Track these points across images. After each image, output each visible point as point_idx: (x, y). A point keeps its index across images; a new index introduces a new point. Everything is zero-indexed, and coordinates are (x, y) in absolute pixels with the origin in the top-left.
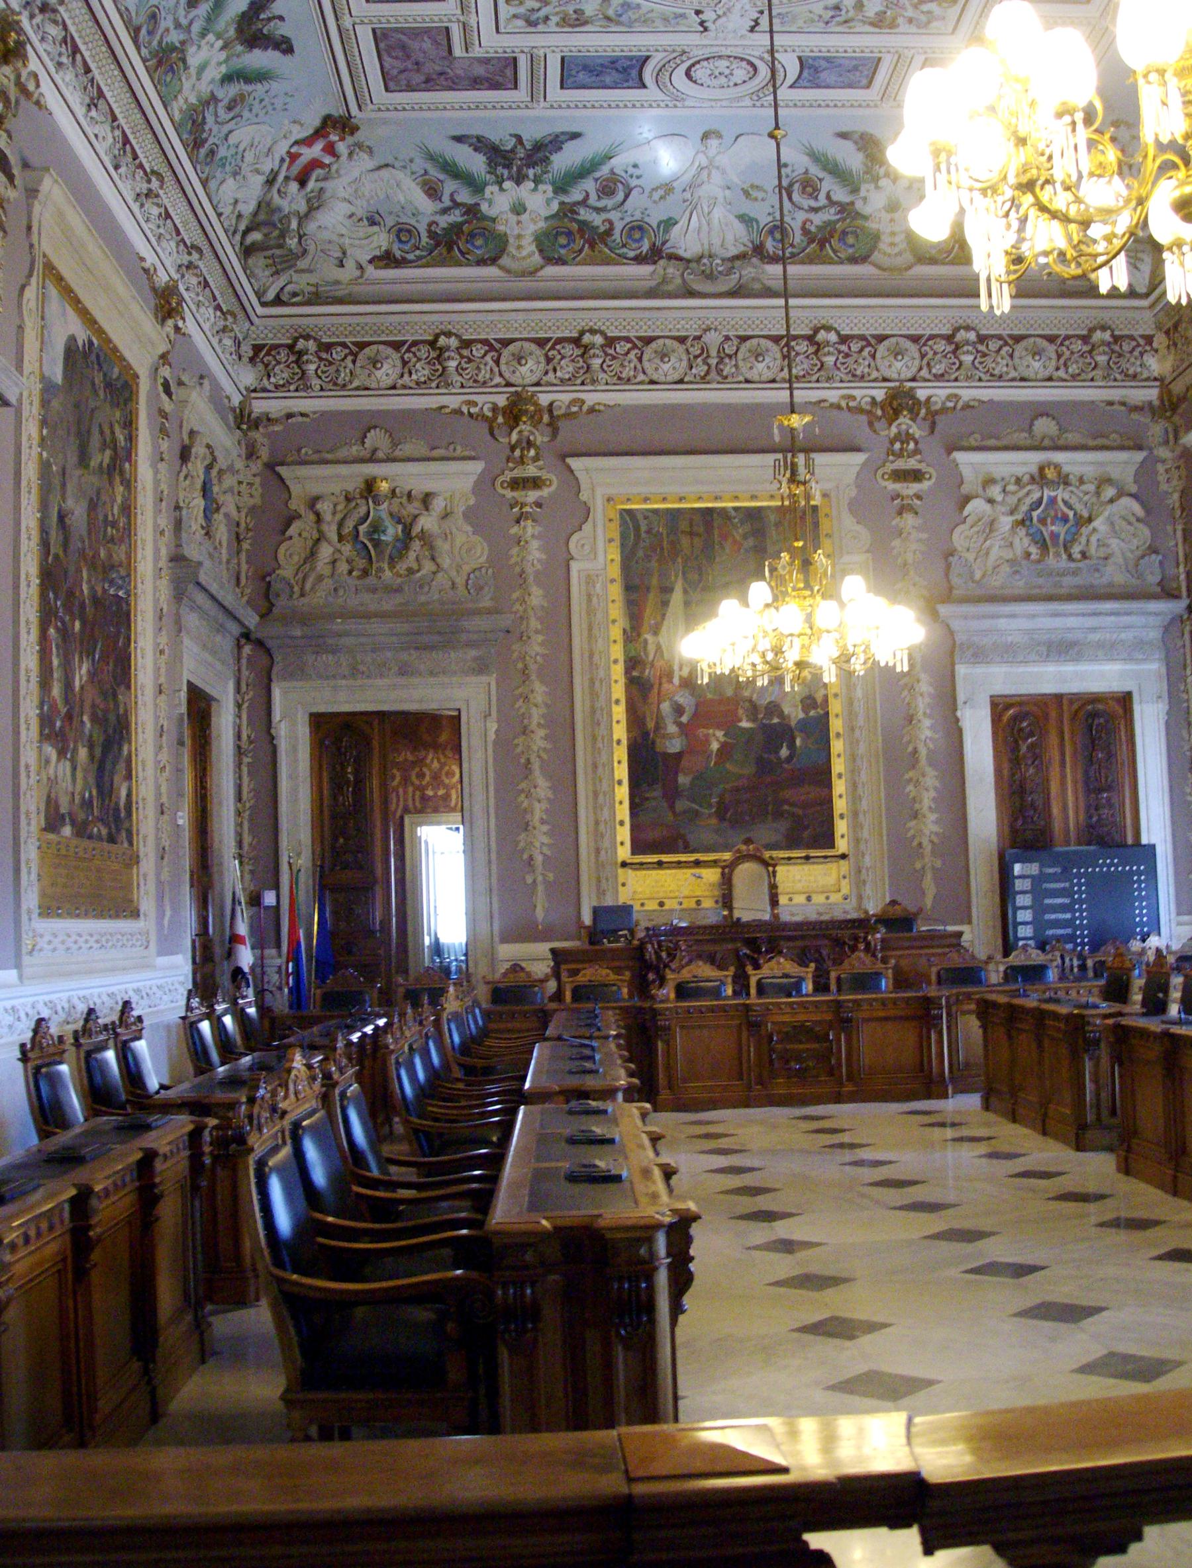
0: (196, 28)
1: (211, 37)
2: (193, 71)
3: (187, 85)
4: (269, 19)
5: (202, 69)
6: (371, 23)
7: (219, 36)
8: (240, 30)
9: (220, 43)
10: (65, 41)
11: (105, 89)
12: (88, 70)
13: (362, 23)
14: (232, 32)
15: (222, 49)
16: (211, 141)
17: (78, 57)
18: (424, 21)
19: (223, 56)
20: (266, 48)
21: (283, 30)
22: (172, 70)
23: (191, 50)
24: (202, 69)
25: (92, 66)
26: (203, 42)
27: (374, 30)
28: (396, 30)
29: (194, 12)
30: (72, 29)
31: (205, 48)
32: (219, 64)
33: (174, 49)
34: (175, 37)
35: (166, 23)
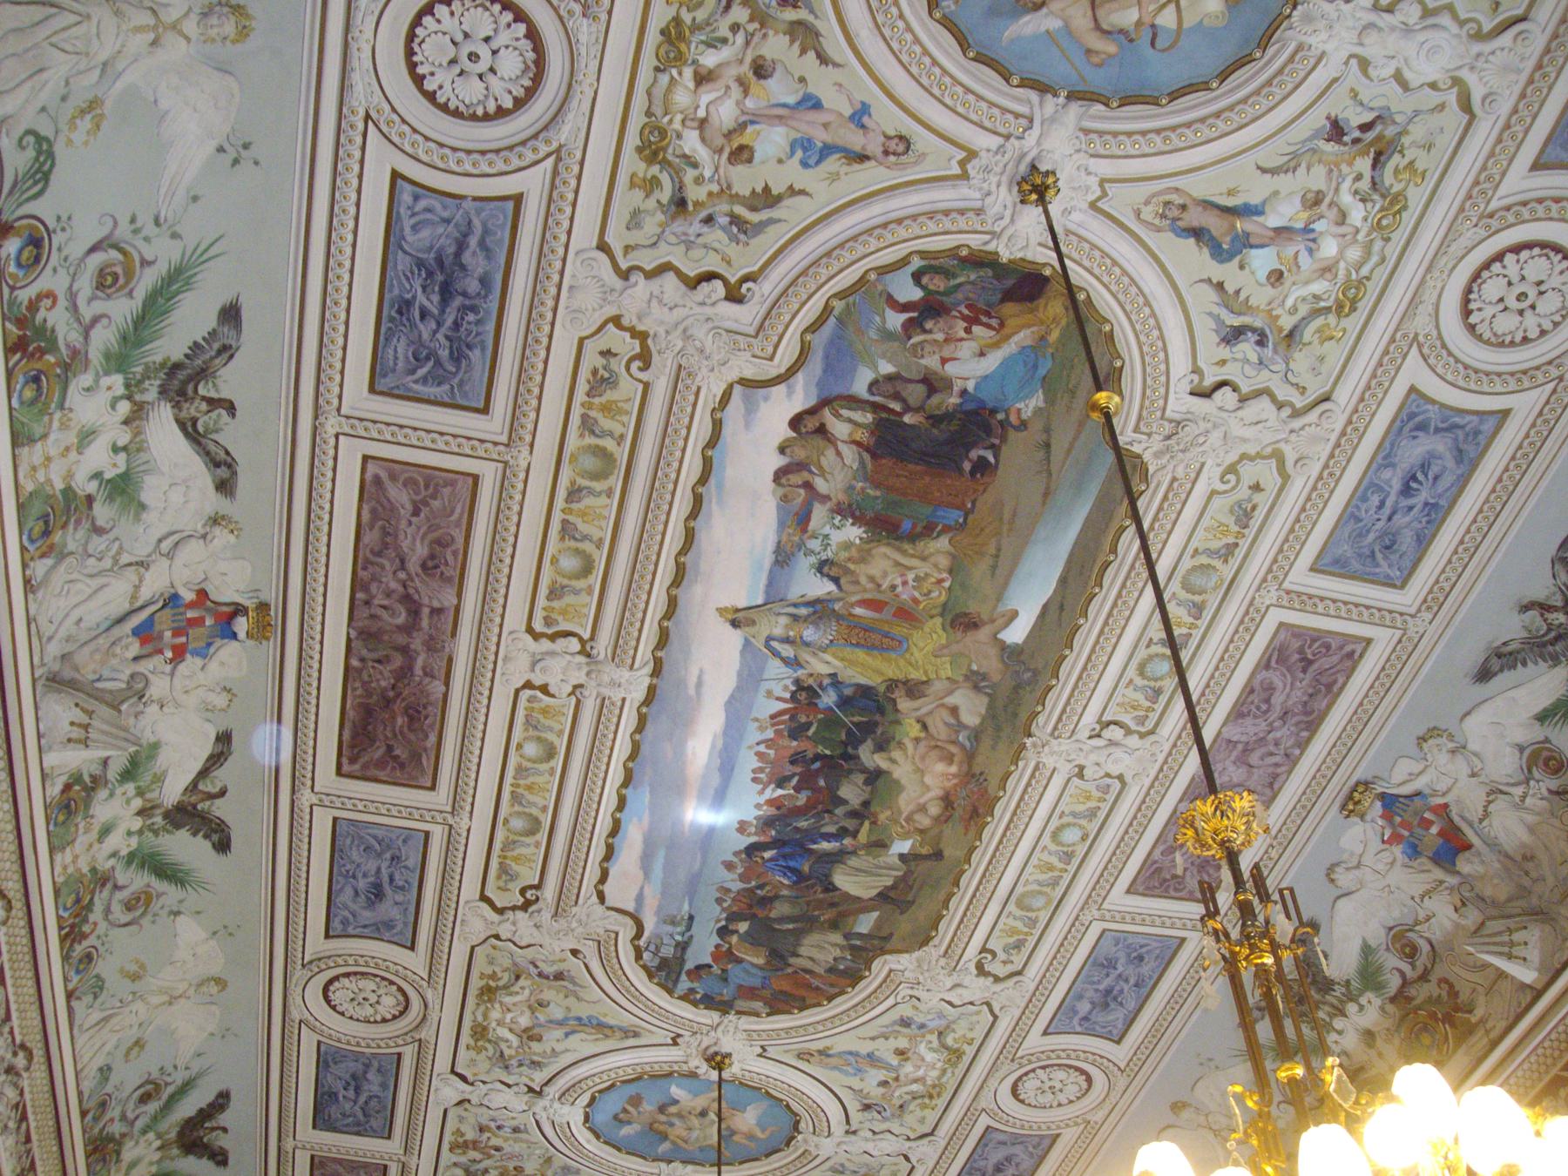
0: (139, 1124)
1: (151, 1135)
2: (124, 1165)
3: (82, 840)
4: (213, 1129)
5: (106, 831)
6: (312, 1149)
7: (159, 1136)
8: (181, 1134)
9: (158, 1143)
10: (17, 1106)
11: (38, 1163)
12: (28, 1140)
13: (304, 1148)
14: (173, 1135)
15: (159, 1149)
16: (92, 940)
17: (24, 1125)
18: (358, 1044)
19: (158, 1155)
20: (201, 1157)
21: (223, 1141)
22: (104, 1160)
23: (129, 1144)
24: (133, 1165)
25: (34, 1137)
26: (143, 1139)
27: (312, 1157)
28: (334, 1160)
29: (144, 1108)
30: (27, 1096)
31: (142, 1144)
32: (151, 1164)
33: (110, 1139)
34: (117, 1128)
35: (114, 1112)
